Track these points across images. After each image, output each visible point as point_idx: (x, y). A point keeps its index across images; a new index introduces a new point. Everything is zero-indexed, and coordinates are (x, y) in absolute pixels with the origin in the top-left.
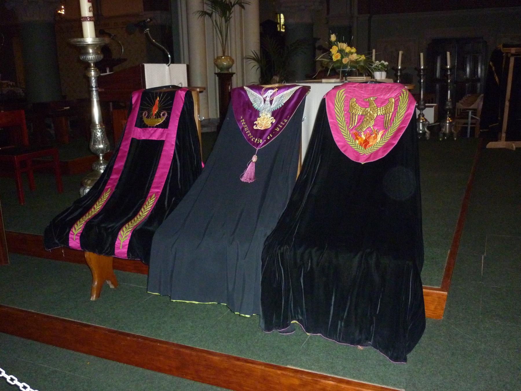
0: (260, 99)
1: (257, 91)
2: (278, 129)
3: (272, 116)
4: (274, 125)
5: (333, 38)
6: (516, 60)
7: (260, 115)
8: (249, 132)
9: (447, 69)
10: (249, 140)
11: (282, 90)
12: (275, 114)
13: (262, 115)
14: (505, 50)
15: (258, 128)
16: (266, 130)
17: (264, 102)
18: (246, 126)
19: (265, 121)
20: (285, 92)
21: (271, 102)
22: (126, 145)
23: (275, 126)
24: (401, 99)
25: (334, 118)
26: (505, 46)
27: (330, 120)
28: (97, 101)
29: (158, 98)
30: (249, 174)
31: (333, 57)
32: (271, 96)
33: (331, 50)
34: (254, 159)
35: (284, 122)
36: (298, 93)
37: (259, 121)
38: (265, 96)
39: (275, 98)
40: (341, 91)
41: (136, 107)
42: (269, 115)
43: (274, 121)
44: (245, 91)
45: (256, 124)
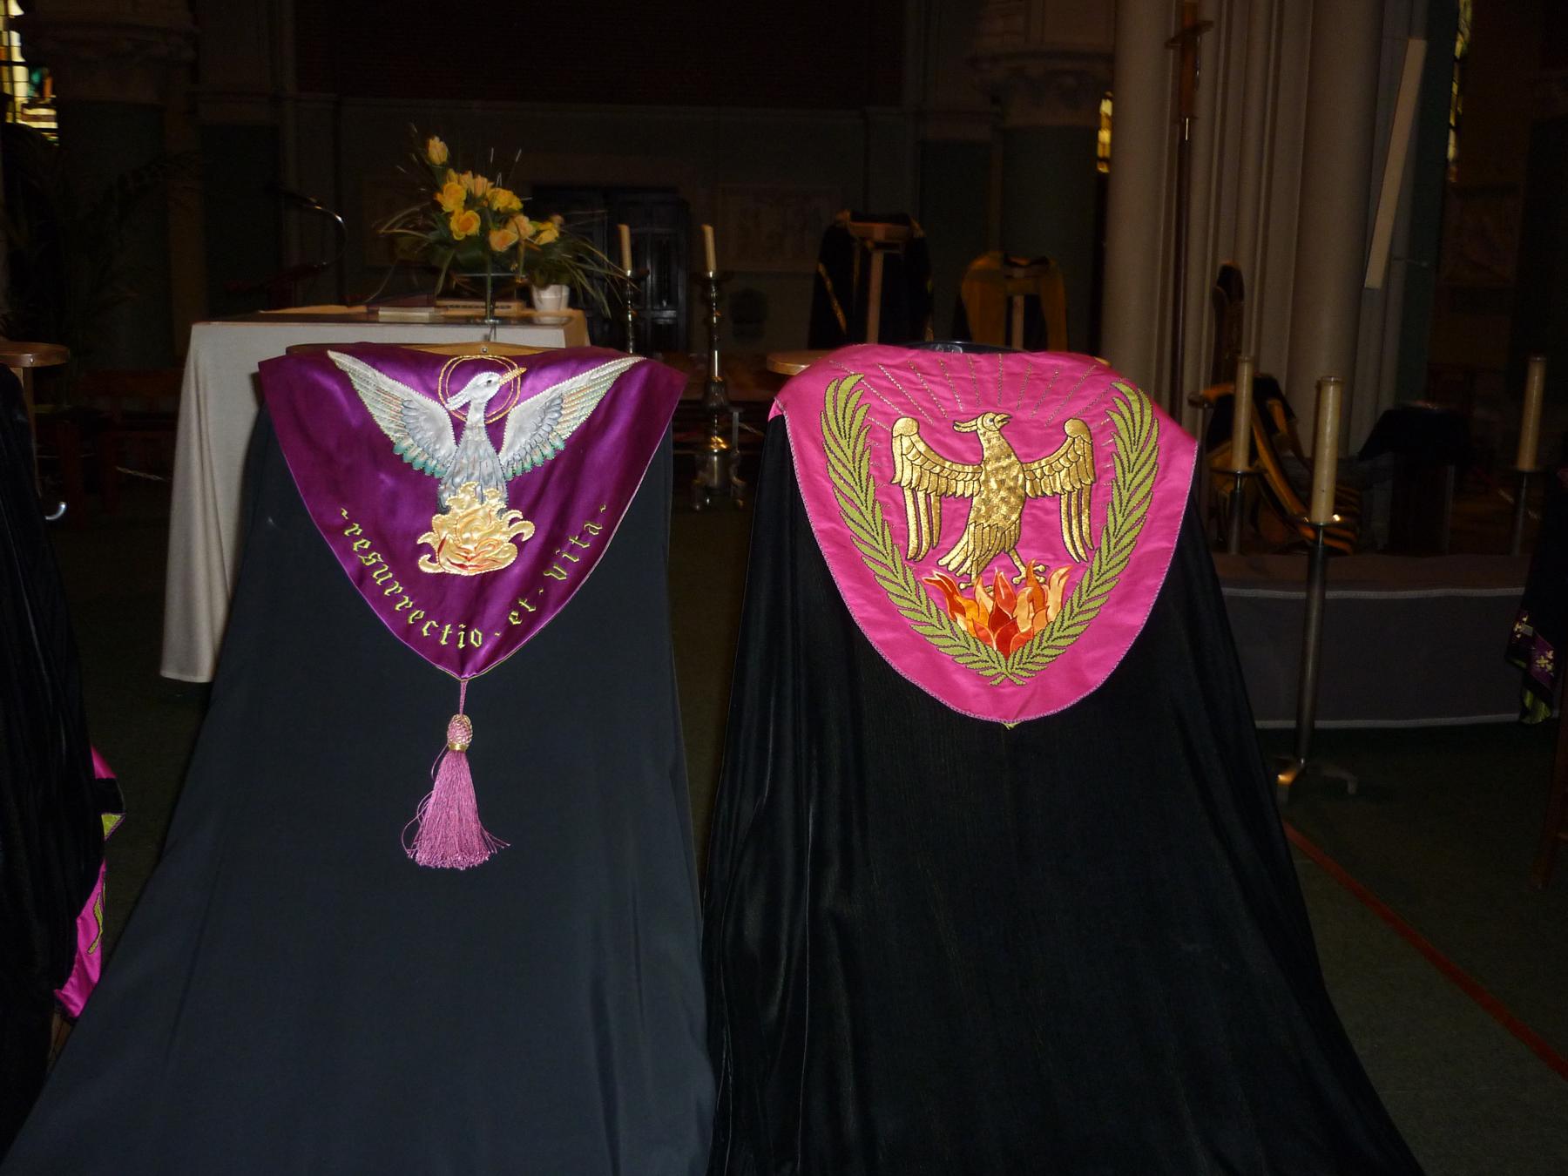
0: (431, 418)
1: (413, 379)
2: (560, 574)
3: (512, 505)
4: (533, 550)
5: (437, 150)
6: (889, 263)
7: (447, 499)
8: (397, 587)
10: (412, 631)
11: (548, 375)
12: (524, 493)
13: (459, 502)
14: (856, 229)
15: (446, 565)
16: (487, 582)
17: (458, 437)
18: (372, 559)
19: (476, 532)
20: (567, 385)
21: (495, 432)
23: (538, 556)
24: (1120, 424)
25: (830, 512)
26: (856, 217)
27: (817, 525)
30: (449, 821)
31: (454, 226)
32: (490, 404)
33: (439, 197)
34: (459, 735)
35: (583, 535)
36: (633, 391)
37: (440, 531)
38: (455, 403)
39: (515, 414)
40: (848, 384)
42: (496, 501)
43: (528, 530)
44: (343, 378)
45: (427, 548)
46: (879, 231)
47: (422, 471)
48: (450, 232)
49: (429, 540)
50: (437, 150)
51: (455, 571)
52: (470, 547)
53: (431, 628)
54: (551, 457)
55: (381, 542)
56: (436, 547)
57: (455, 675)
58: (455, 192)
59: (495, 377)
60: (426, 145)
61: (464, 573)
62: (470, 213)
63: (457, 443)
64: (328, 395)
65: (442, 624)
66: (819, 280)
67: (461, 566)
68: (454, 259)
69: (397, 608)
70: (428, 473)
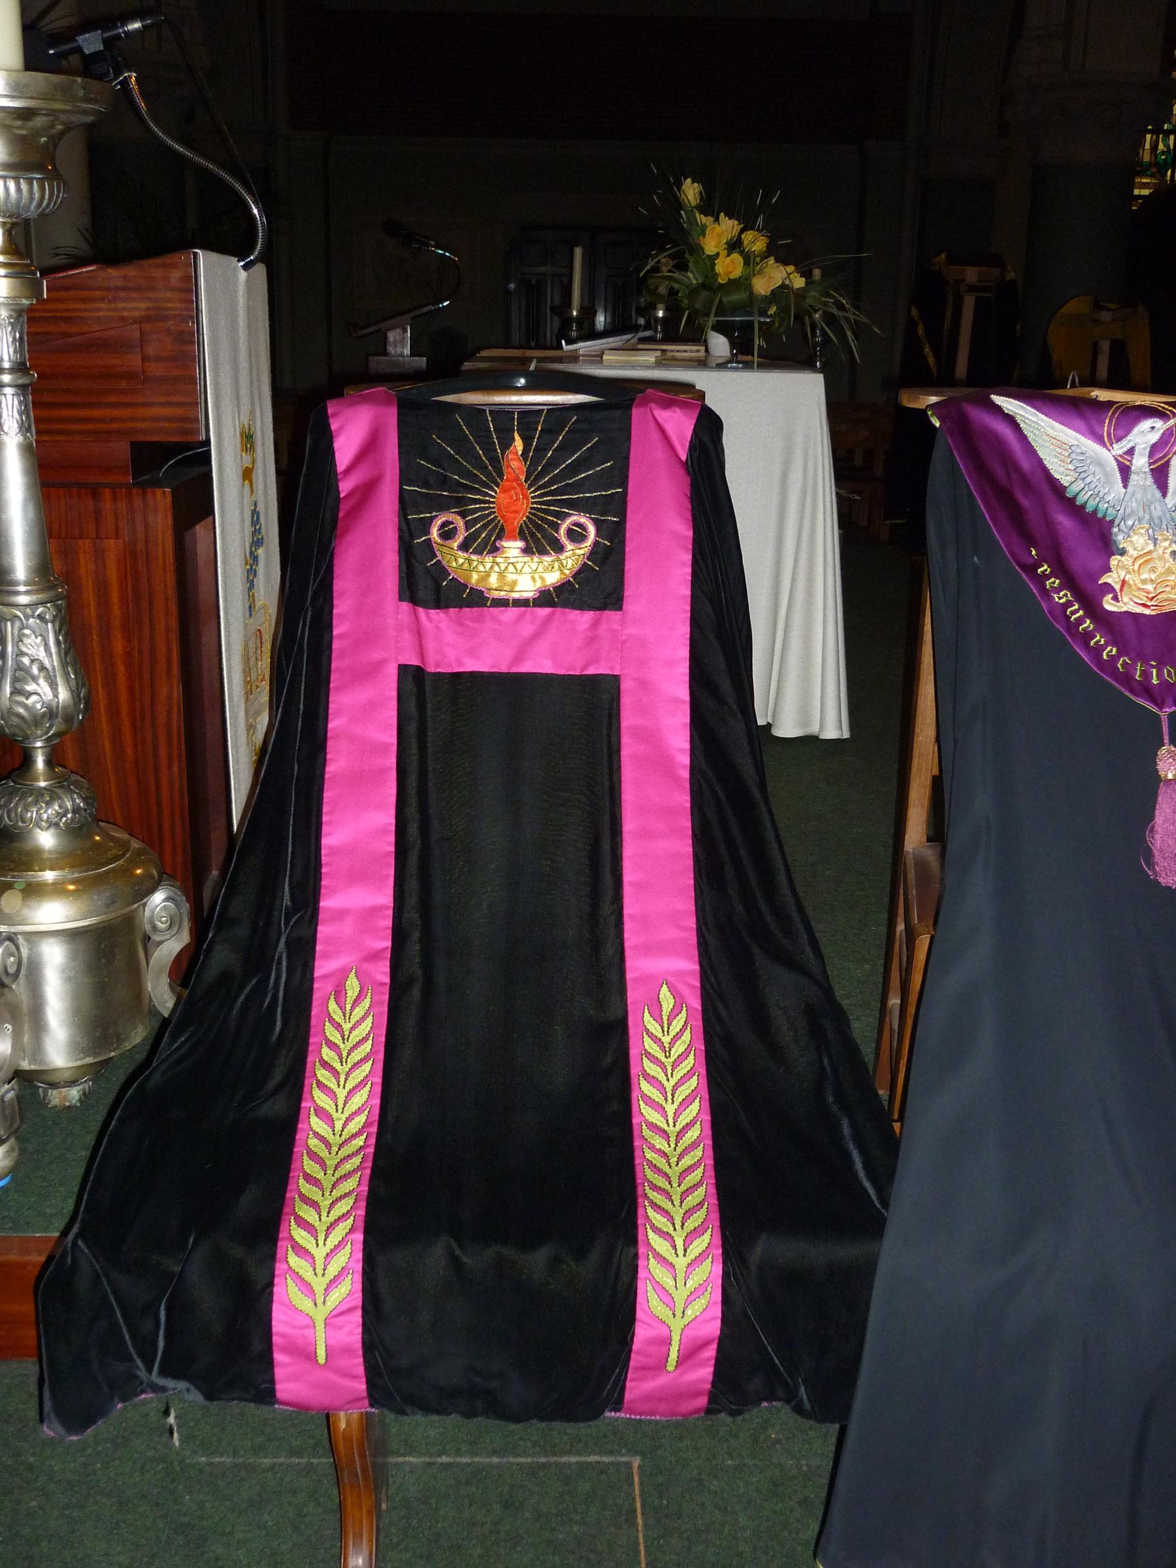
0: (1099, 463)
1: (1080, 424)
7: (1120, 538)
9: (571, 318)
15: (1127, 604)
21: (1160, 475)
22: (371, 707)
28: (27, 450)
29: (519, 444)
31: (719, 268)
32: (1154, 449)
38: (1119, 448)
41: (367, 490)
45: (1108, 588)
46: (972, 274)
47: (1095, 512)
48: (716, 275)
49: (1109, 581)
50: (691, 191)
51: (1139, 610)
52: (1150, 587)
53: (1125, 664)
54: (1080, 501)
55: (1070, 582)
56: (1117, 587)
57: (1154, 709)
58: (717, 234)
59: (1158, 423)
60: (679, 185)
61: (1147, 612)
62: (735, 256)
63: (1125, 486)
64: (999, 444)
65: (1134, 662)
66: (911, 325)
67: (1144, 605)
68: (721, 302)
69: (1092, 643)
70: (1100, 515)
